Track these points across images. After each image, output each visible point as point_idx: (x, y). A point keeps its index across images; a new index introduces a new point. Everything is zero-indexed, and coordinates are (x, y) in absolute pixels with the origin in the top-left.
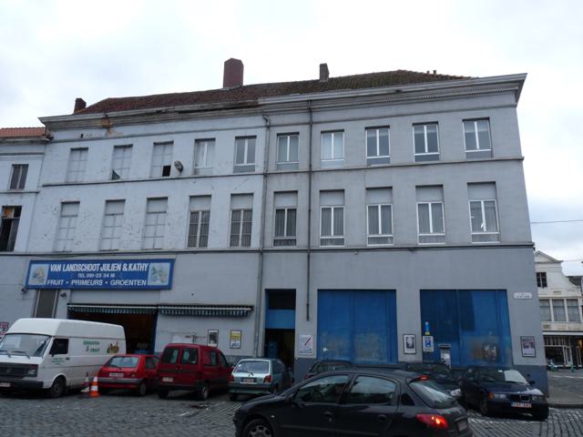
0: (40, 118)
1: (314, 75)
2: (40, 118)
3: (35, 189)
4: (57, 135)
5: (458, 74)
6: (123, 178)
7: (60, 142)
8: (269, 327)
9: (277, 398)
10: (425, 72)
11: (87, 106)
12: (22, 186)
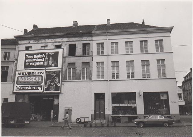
0: (14, 36)
1: (105, 22)
2: (14, 36)
3: (13, 60)
4: (20, 42)
5: (158, 26)
6: (16, 58)
7: (21, 44)
8: (58, 100)
9: (146, 120)
10: (71, 25)
11: (28, 31)
12: (8, 59)
